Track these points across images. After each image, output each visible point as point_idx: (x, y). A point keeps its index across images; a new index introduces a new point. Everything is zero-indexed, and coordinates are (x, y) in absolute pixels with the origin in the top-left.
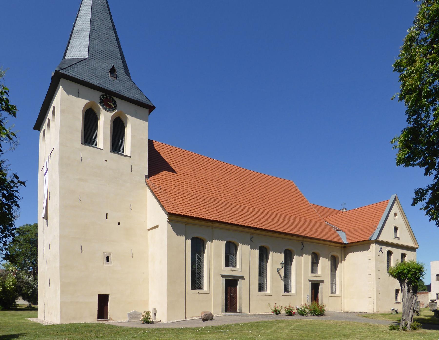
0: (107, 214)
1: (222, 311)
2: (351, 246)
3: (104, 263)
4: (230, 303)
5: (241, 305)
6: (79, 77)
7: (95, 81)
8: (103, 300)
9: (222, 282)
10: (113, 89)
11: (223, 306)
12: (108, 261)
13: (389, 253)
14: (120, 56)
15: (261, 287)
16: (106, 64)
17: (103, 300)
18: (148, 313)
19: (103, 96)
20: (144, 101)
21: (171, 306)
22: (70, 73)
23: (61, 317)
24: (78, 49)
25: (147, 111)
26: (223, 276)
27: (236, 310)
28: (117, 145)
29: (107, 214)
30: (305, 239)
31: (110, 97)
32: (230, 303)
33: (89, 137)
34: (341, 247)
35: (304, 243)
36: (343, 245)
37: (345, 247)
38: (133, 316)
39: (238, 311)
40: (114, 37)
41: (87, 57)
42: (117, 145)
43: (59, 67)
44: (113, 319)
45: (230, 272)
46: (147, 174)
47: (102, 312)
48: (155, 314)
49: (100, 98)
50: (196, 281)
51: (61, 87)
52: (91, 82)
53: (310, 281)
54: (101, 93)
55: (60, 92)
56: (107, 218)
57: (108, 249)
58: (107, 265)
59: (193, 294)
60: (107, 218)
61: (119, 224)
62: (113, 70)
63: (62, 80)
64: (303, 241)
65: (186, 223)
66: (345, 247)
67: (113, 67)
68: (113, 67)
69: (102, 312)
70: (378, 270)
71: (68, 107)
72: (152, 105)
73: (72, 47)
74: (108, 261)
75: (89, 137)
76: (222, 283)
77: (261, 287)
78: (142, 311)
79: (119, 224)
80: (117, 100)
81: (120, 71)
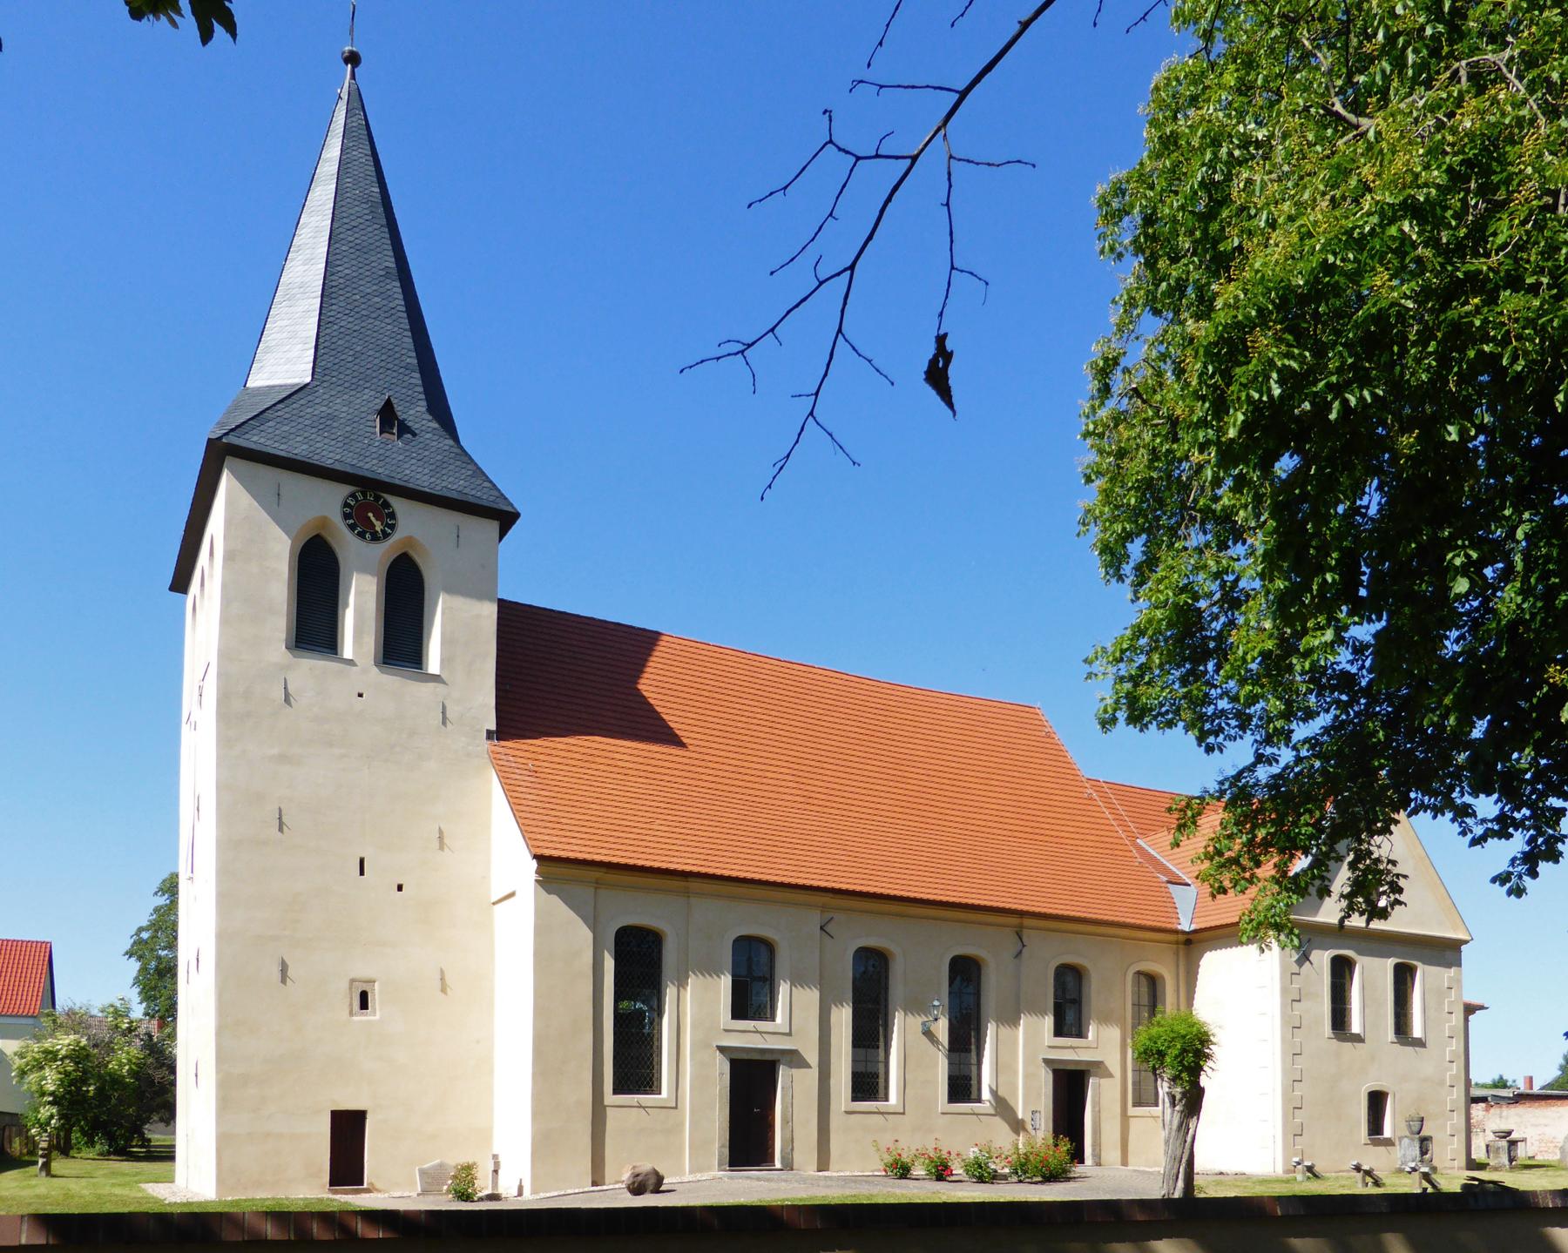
0: (362, 861)
1: (720, 1164)
2: (1200, 941)
3: (351, 1014)
4: (749, 1141)
5: (789, 1142)
6: (280, 449)
7: (329, 456)
8: (348, 1131)
9: (721, 1070)
10: (382, 472)
11: (722, 1146)
12: (364, 1005)
13: (1342, 970)
14: (415, 361)
15: (867, 1085)
16: (367, 394)
17: (348, 1131)
18: (468, 1170)
19: (353, 495)
20: (484, 497)
21: (544, 1146)
22: (254, 440)
23: (220, 1181)
24: (285, 357)
25: (493, 527)
26: (722, 1049)
27: (772, 1161)
28: (401, 644)
29: (362, 861)
30: (1028, 922)
31: (377, 498)
32: (749, 1141)
33: (314, 627)
34: (1177, 943)
35: (1026, 934)
36: (1182, 938)
37: (1188, 942)
38: (431, 1179)
39: (778, 1165)
40: (399, 301)
41: (308, 379)
42: (401, 644)
43: (220, 424)
44: (378, 1185)
45: (752, 1036)
46: (493, 727)
47: (347, 1160)
48: (496, 1171)
49: (346, 505)
50: (635, 1065)
51: (255, 381)
52: (316, 459)
53: (1047, 1062)
54: (344, 490)
55: (226, 483)
56: (362, 873)
57: (362, 970)
58: (362, 1018)
59: (624, 1110)
60: (362, 873)
61: (400, 888)
62: (388, 416)
63: (229, 460)
64: (1021, 927)
65: (598, 884)
66: (1188, 942)
67: (388, 403)
68: (388, 403)
69: (347, 1160)
70: (1293, 1027)
71: (247, 539)
72: (509, 509)
73: (268, 351)
74: (364, 1005)
75: (314, 627)
76: (722, 1074)
77: (867, 1085)
78: (455, 1158)
79: (400, 888)
80: (397, 503)
81: (415, 412)
